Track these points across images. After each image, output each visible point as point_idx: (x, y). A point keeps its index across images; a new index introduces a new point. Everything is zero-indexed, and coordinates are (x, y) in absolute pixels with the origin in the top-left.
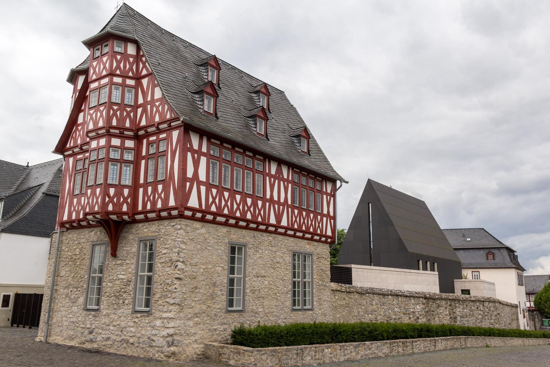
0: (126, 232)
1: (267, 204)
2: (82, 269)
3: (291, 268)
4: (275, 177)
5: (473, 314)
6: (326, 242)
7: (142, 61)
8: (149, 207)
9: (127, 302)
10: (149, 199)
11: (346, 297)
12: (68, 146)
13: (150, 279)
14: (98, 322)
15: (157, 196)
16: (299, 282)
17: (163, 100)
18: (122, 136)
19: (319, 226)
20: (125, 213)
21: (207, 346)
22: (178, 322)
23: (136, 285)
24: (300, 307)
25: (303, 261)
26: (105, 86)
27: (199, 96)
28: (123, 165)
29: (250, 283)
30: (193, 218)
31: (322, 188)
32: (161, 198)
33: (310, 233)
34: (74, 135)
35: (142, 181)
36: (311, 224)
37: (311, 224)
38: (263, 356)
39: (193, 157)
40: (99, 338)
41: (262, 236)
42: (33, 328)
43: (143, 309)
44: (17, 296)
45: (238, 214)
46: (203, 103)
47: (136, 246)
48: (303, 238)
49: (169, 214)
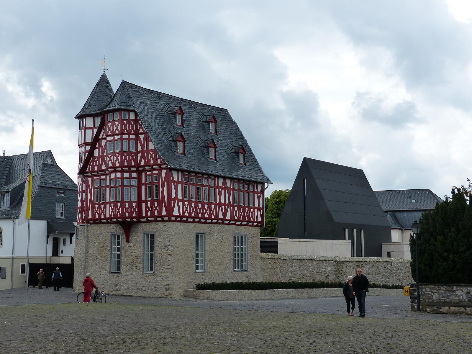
0: (134, 228)
1: (217, 206)
2: (106, 248)
3: (233, 245)
4: (222, 188)
5: (379, 272)
6: (257, 226)
7: (139, 123)
8: (149, 214)
9: (138, 268)
10: (149, 210)
11: (272, 262)
12: (87, 170)
13: (152, 256)
14: (120, 280)
15: (154, 208)
16: (238, 254)
17: (155, 151)
18: (130, 172)
19: (252, 216)
20: (135, 218)
21: (186, 291)
22: (171, 278)
23: (144, 259)
24: (239, 270)
25: (241, 240)
26: (118, 140)
27: (174, 143)
28: (131, 188)
29: (208, 256)
30: (176, 221)
31: (254, 189)
32: (157, 210)
34: (92, 164)
35: (143, 198)
37: (247, 215)
38: (217, 294)
40: (122, 288)
42: (48, 287)
43: (150, 272)
44: (31, 265)
46: (177, 148)
47: (142, 236)
48: (241, 225)
49: (163, 219)
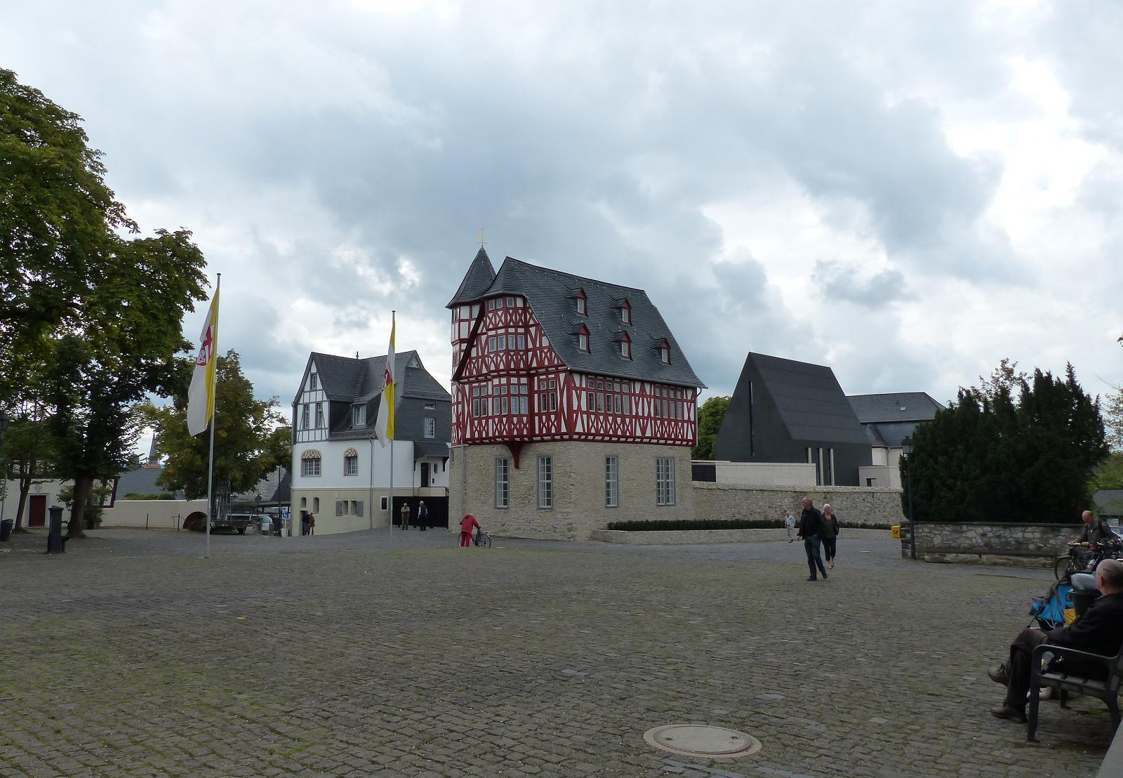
4: (639, 396)
6: (687, 445)
8: (544, 432)
12: (464, 375)
16: (662, 483)
17: (550, 348)
23: (538, 489)
31: (682, 397)
32: (555, 426)
33: (672, 439)
35: (536, 411)
36: (673, 431)
37: (673, 431)
39: (577, 393)
41: (630, 446)
45: (611, 433)
48: (665, 444)
49: (562, 437)
